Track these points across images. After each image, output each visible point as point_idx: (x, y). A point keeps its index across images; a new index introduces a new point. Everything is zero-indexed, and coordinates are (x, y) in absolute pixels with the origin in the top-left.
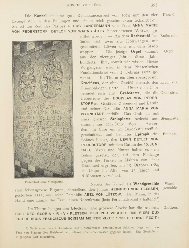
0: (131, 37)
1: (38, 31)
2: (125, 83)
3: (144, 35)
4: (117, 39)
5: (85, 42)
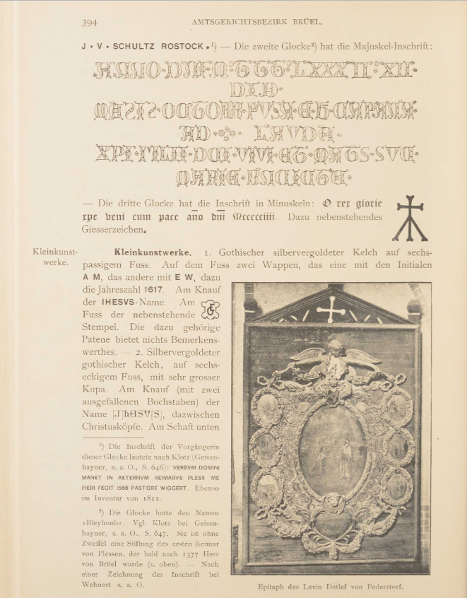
0: (99, 275)
1: (180, 46)
2: (89, 544)
3: (160, 252)
4: (153, 570)
5: (138, 278)
